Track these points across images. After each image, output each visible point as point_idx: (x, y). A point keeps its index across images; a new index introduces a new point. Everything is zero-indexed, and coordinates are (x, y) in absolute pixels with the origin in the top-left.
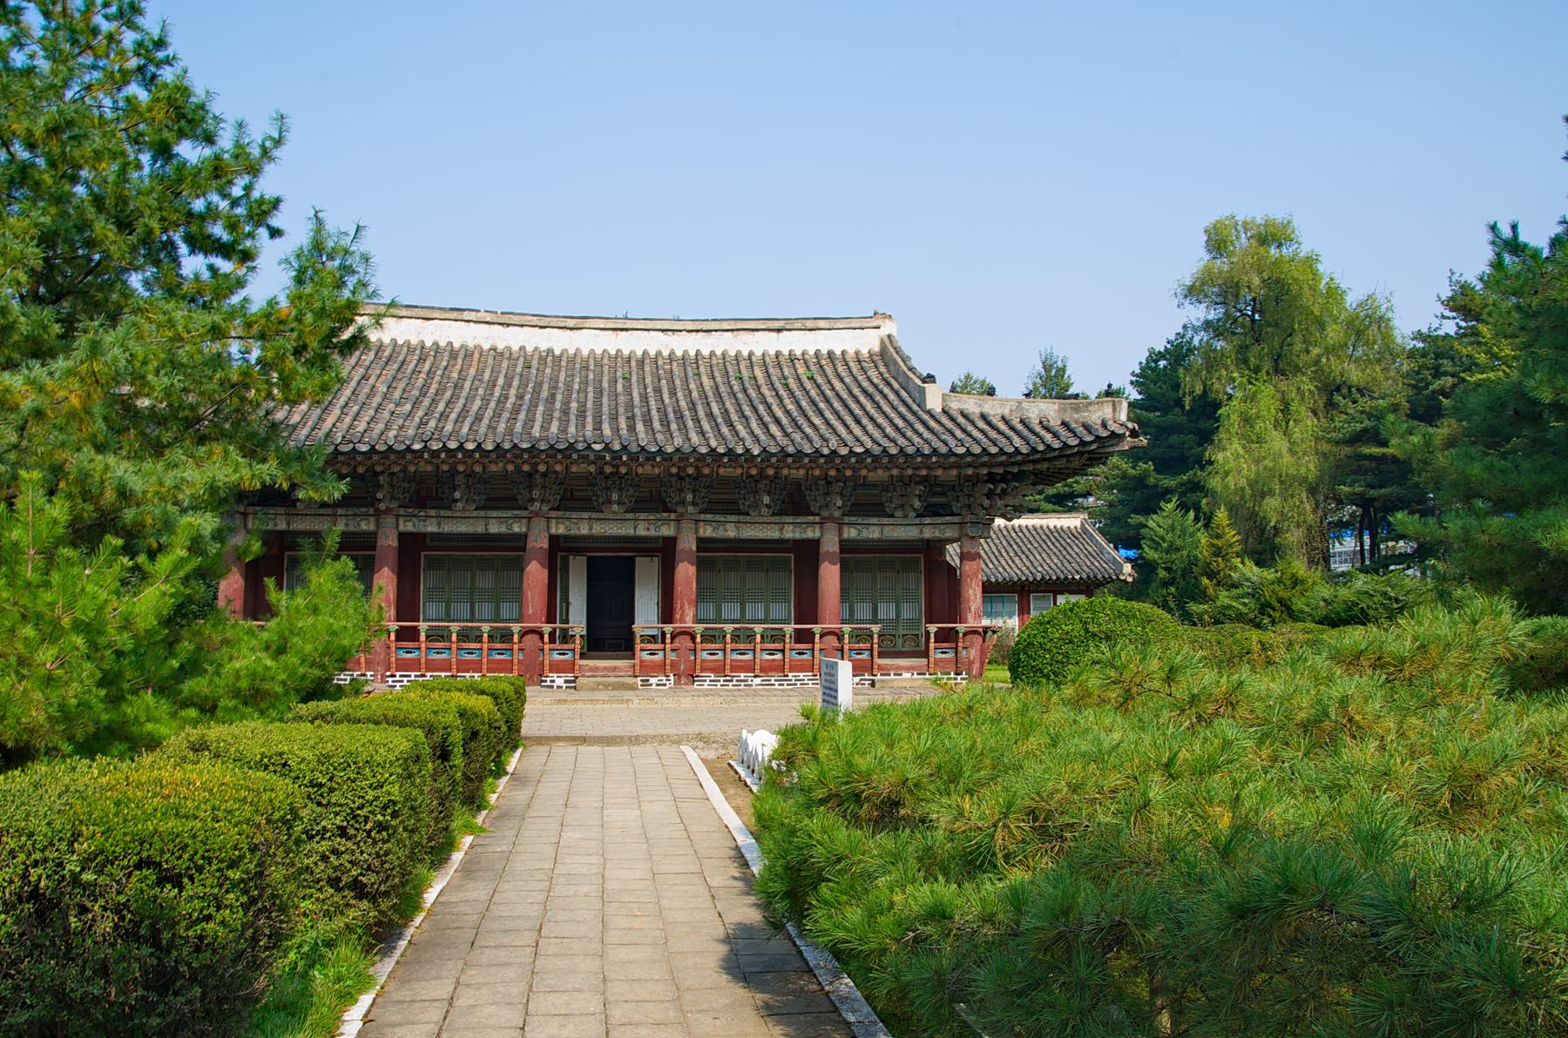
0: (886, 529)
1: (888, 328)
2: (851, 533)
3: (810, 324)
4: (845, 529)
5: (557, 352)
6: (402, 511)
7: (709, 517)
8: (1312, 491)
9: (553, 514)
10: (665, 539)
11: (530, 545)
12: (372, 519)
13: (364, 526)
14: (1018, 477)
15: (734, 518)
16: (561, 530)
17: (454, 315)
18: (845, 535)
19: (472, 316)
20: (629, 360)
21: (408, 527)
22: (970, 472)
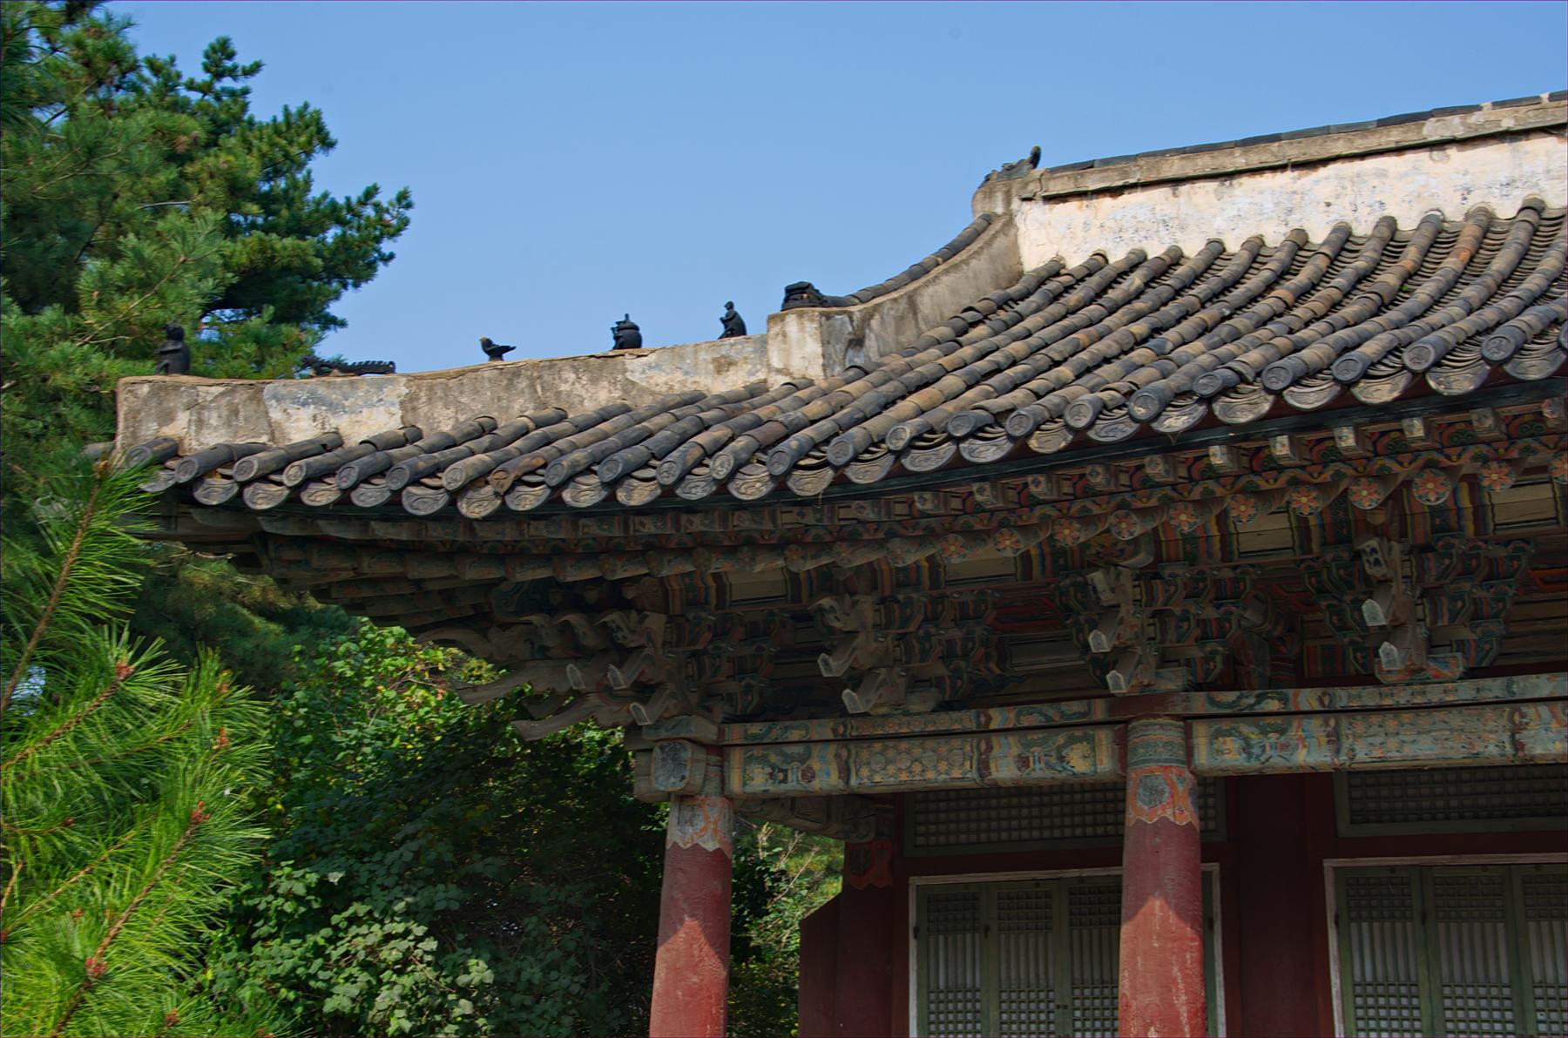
6: (1199, 703)
17: (1394, 136)
19: (1455, 126)
21: (1225, 753)
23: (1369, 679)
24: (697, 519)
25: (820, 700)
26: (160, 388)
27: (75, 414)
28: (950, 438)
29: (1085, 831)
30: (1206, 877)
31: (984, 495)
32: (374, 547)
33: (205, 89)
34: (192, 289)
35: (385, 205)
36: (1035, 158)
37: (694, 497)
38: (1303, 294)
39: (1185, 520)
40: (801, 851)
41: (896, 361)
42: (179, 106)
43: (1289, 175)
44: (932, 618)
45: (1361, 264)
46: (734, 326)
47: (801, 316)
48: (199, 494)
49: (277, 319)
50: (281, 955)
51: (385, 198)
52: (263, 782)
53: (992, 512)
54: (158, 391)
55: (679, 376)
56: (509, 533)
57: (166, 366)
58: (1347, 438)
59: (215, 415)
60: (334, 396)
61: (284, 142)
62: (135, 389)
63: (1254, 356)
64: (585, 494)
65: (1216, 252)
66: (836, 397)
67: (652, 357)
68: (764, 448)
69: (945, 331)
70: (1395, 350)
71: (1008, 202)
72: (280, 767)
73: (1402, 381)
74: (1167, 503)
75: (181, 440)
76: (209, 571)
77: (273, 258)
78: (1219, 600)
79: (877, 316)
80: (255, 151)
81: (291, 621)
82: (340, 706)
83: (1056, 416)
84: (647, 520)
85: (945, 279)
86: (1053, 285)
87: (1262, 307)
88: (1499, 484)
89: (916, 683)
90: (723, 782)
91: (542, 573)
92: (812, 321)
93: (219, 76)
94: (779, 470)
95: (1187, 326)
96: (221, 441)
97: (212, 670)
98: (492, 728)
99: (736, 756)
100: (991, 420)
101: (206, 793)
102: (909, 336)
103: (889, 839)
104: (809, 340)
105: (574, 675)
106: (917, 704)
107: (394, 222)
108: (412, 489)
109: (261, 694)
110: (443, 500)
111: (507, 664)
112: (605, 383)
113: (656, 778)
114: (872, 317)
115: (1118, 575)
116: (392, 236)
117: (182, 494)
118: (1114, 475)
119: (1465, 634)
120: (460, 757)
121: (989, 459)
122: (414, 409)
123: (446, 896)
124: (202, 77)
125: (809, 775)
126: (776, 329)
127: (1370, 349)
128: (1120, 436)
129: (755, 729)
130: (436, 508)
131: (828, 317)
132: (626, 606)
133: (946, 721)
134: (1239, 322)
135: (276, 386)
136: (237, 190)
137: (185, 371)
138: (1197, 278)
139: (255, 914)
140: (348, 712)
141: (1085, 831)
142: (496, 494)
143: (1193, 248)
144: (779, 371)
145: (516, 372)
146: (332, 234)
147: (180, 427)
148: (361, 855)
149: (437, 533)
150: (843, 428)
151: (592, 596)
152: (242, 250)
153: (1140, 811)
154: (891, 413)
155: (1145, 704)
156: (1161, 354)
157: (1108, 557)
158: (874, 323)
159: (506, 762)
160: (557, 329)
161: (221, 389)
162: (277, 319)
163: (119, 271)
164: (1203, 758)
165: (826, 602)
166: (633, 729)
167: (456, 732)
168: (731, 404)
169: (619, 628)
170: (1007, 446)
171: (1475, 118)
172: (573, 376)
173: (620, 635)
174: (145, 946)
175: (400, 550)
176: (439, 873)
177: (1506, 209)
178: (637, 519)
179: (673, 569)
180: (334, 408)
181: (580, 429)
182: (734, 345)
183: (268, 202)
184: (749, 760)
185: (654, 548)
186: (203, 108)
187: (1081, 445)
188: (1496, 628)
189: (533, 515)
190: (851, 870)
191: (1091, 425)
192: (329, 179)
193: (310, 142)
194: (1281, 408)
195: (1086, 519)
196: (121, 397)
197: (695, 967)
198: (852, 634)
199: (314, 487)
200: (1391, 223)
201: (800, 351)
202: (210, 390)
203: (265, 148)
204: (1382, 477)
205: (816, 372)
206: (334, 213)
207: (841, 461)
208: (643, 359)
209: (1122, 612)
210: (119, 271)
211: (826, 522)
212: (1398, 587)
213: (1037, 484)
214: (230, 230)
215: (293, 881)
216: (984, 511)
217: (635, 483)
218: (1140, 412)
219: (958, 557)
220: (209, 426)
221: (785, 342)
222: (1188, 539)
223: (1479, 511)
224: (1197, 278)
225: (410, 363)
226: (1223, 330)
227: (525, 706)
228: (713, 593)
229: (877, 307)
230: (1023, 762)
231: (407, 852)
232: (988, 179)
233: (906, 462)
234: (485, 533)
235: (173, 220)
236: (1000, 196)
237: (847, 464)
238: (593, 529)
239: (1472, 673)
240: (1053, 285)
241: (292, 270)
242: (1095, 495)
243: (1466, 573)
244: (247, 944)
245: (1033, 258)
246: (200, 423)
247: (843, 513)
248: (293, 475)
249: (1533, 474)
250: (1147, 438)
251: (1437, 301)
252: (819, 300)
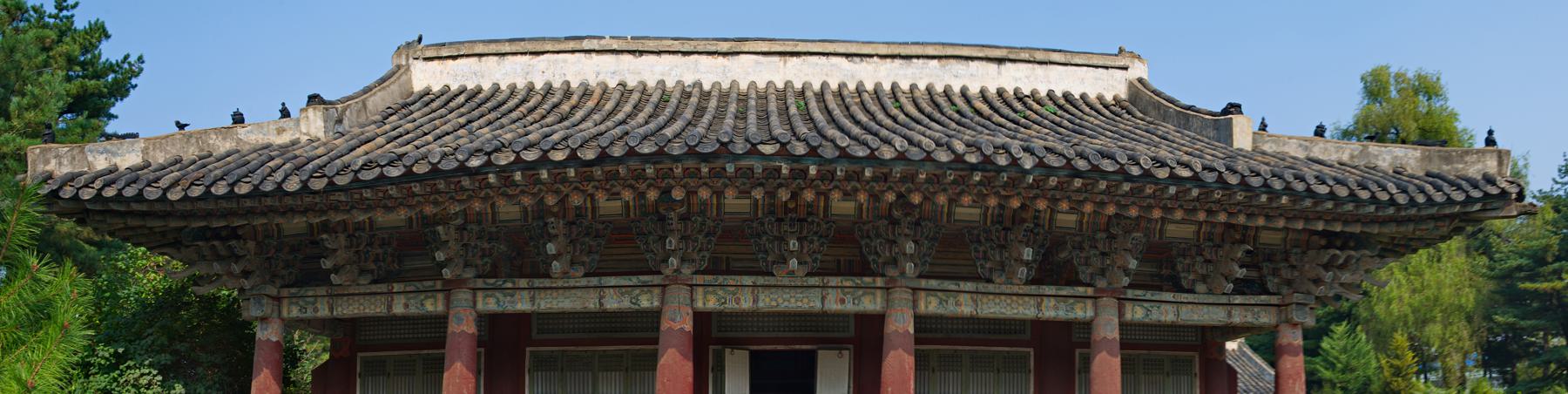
0: (1184, 309)
1: (1138, 70)
2: (1136, 313)
3: (1040, 56)
4: (1128, 306)
5: (707, 87)
6: (480, 283)
7: (933, 283)
8: (1469, 319)
9: (699, 279)
10: (862, 318)
11: (665, 325)
12: (440, 296)
13: (429, 307)
14: (1360, 242)
15: (969, 286)
16: (712, 304)
17: (571, 45)
18: (1128, 316)
19: (594, 44)
20: (802, 93)
21: (489, 304)
22: (1320, 226)
23: (549, 276)
25: (322, 278)
27: (11, 163)
29: (432, 333)
30: (479, 354)
31: (393, 191)
33: (56, 17)
34: (55, 106)
36: (420, 39)
38: (531, 111)
39: (477, 206)
40: (312, 342)
41: (357, 130)
42: (46, 26)
43: (528, 57)
44: (370, 244)
45: (555, 100)
46: (285, 113)
49: (89, 117)
50: (101, 381)
51: (132, 59)
52: (91, 312)
54: (43, 151)
56: (189, 207)
58: (544, 175)
62: (34, 151)
63: (509, 136)
64: (220, 189)
65: (496, 89)
66: (330, 146)
68: (298, 168)
69: (379, 117)
70: (565, 139)
72: (98, 306)
73: (567, 152)
74: (470, 198)
76: (66, 226)
78: (490, 240)
81: (99, 245)
82: (120, 280)
83: (424, 157)
86: (426, 99)
87: (514, 115)
88: (601, 197)
89: (362, 272)
90: (280, 312)
91: (203, 224)
95: (482, 121)
97: (69, 267)
98: (183, 289)
99: (285, 302)
101: (69, 316)
102: (363, 119)
103: (349, 337)
105: (217, 267)
106: (363, 281)
109: (89, 276)
111: (189, 263)
113: (251, 311)
117: (54, 194)
118: (448, 184)
119: (585, 259)
120: (170, 302)
123: (165, 358)
124: (54, 11)
125: (316, 310)
127: (556, 137)
129: (293, 290)
132: (238, 237)
133: (374, 288)
134: (504, 120)
136: (71, 61)
137: (53, 142)
138: (487, 100)
139: (90, 364)
140: (124, 283)
141: (432, 333)
143: (487, 86)
145: (191, 135)
146: (111, 77)
147: (52, 166)
148: (131, 342)
149: (158, 207)
150: (332, 160)
151: (224, 233)
152: (74, 87)
153: (453, 327)
154: (354, 153)
155: (458, 283)
156: (471, 133)
157: (445, 220)
159: (188, 304)
160: (208, 116)
162: (89, 117)
163: (25, 101)
164: (480, 306)
165: (324, 236)
166: (241, 290)
167: (168, 291)
168: (284, 149)
170: (403, 170)
171: (603, 42)
174: (48, 376)
176: (162, 349)
177: (612, 84)
179: (259, 221)
180: (114, 154)
181: (218, 160)
182: (285, 122)
183: (83, 65)
184: (291, 304)
185: (251, 212)
186: (56, 26)
187: (435, 171)
188: (597, 257)
189: (198, 199)
190: (333, 350)
192: (109, 52)
194: (518, 160)
195: (436, 203)
197: (267, 389)
198: (335, 250)
200: (568, 83)
201: (314, 125)
202: (63, 149)
204: (557, 192)
205: (321, 135)
206: (111, 68)
210: (25, 101)
212: (561, 238)
214: (69, 79)
215: (105, 352)
218: (460, 157)
219: (381, 218)
222: (478, 214)
223: (594, 209)
224: (487, 100)
225: (144, 134)
226: (497, 124)
227: (196, 280)
230: (406, 306)
231: (149, 340)
234: (179, 207)
235: (46, 77)
238: (224, 204)
239: (586, 275)
240: (426, 99)
241: (96, 93)
243: (587, 234)
244: (87, 376)
245: (418, 86)
246: (60, 164)
248: (98, 184)
249: (614, 196)
250: (463, 169)
251: (583, 120)
252: (323, 102)
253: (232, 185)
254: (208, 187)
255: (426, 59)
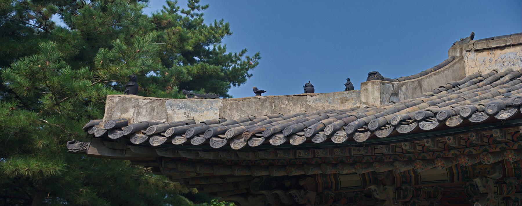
24: (320, 151)
26: (123, 99)
28: (415, 121)
31: (429, 144)
32: (202, 162)
33: (188, 13)
35: (251, 58)
36: (472, 37)
37: (318, 142)
47: (373, 83)
48: (133, 141)
53: (434, 152)
54: (122, 100)
55: (327, 104)
56: (251, 157)
57: (128, 91)
59: (145, 111)
60: (194, 106)
61: (214, 32)
64: (278, 141)
67: (317, 97)
71: (461, 52)
75: (130, 120)
77: (206, 72)
79: (405, 86)
80: (203, 35)
84: (302, 152)
85: (434, 76)
92: (377, 85)
93: (193, 9)
94: (350, 132)
96: (146, 121)
100: (433, 115)
104: (376, 92)
107: (253, 64)
108: (214, 139)
110: (225, 142)
112: (299, 105)
114: (402, 86)
115: (487, 181)
116: (252, 68)
121: (430, 129)
122: (224, 112)
124: (187, 9)
126: (364, 88)
128: (481, 120)
130: (222, 146)
131: (383, 84)
132: (300, 188)
135: (172, 101)
142: (245, 140)
144: (364, 103)
145: (265, 100)
149: (223, 156)
151: (288, 184)
158: (403, 88)
161: (148, 101)
169: (296, 196)
170: (437, 124)
172: (287, 102)
173: (296, 199)
175: (212, 164)
178: (298, 151)
180: (193, 110)
191: (470, 116)
193: (223, 32)
195: (471, 156)
196: (107, 101)
199: (177, 137)
203: (206, 34)
205: (378, 104)
207: (373, 129)
208: (314, 97)
209: (489, 196)
210: (111, 54)
211: (369, 154)
213: (449, 140)
216: (430, 151)
217: (297, 137)
220: (142, 115)
221: (367, 93)
228: (334, 184)
229: (406, 83)
232: (454, 44)
233: (398, 130)
236: (458, 50)
237: (376, 130)
242: (474, 146)
247: (376, 151)
248: (169, 133)
252: (382, 78)
253: (288, 137)
254: (268, 139)
255: (477, 51)
